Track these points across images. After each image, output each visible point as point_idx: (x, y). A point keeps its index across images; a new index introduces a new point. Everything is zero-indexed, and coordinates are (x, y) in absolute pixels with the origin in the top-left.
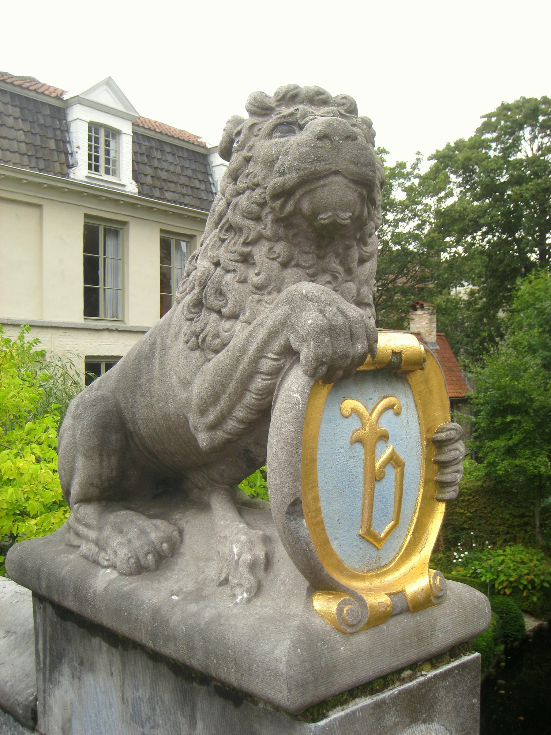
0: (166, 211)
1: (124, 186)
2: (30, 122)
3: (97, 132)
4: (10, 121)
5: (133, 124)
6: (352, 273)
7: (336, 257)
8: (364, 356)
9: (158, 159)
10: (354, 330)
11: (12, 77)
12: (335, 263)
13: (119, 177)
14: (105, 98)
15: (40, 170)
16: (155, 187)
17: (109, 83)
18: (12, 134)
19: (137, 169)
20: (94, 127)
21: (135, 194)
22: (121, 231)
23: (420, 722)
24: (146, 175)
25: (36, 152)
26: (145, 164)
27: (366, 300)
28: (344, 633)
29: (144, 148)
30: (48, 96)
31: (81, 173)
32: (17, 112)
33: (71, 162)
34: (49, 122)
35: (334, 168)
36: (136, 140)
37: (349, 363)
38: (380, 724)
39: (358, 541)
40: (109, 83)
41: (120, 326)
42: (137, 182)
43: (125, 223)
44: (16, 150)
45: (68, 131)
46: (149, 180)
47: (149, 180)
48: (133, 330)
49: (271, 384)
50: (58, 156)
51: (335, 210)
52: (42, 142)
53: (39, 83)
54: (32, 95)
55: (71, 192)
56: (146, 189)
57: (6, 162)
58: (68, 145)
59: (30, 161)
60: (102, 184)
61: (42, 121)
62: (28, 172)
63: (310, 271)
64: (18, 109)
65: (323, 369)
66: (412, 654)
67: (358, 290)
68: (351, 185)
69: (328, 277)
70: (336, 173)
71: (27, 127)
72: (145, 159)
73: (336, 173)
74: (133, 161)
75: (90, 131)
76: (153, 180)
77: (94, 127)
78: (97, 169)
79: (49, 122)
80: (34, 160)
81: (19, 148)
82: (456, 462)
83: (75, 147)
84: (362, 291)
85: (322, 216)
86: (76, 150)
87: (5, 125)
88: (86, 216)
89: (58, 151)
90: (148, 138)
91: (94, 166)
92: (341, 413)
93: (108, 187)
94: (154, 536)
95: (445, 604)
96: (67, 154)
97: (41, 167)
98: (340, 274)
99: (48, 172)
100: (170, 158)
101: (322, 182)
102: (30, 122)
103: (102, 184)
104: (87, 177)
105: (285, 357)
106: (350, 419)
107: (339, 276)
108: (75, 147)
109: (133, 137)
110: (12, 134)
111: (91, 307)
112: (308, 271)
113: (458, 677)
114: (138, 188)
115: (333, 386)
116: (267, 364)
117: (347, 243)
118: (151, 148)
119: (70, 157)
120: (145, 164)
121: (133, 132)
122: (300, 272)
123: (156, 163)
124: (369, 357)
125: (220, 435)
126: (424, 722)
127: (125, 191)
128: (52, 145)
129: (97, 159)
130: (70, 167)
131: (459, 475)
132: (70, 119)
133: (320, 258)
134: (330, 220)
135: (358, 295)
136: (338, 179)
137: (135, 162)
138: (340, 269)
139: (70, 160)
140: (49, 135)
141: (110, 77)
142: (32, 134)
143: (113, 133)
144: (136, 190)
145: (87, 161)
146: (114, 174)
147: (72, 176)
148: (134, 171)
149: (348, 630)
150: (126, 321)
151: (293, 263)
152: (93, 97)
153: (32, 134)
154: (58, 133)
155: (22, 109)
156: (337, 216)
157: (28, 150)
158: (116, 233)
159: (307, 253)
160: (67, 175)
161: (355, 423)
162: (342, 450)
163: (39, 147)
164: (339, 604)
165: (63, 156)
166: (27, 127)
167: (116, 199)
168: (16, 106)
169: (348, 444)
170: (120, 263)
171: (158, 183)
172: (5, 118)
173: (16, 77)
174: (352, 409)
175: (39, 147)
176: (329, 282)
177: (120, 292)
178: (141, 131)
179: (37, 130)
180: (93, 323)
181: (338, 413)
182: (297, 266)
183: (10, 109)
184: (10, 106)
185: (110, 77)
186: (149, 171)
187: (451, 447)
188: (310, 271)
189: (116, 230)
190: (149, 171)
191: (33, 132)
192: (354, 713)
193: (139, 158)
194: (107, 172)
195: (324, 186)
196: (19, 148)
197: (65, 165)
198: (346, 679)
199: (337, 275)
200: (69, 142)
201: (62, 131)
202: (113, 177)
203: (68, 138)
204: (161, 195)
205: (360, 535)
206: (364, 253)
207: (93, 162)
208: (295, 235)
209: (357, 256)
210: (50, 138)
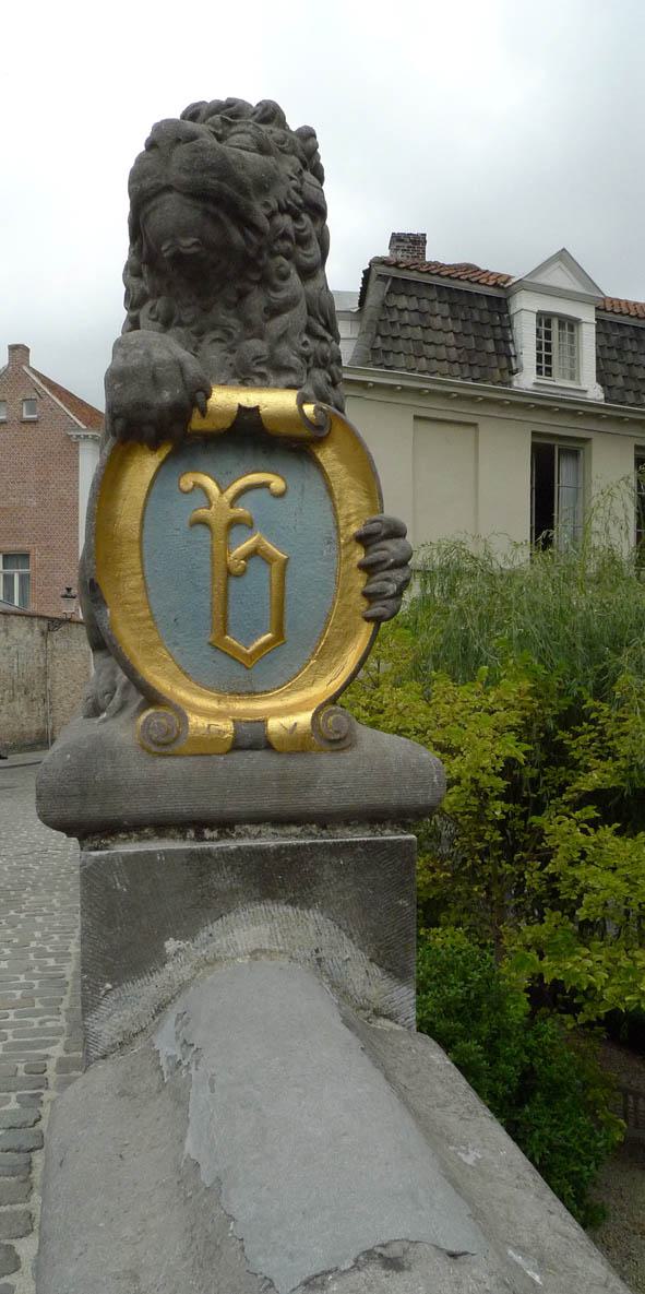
0: (599, 415)
1: (585, 391)
2: (462, 320)
3: (548, 324)
4: (437, 322)
5: (597, 309)
9: (633, 353)
10: (159, 375)
11: (443, 266)
13: (579, 380)
14: (559, 278)
15: (474, 380)
16: (628, 391)
17: (563, 256)
18: (439, 338)
19: (602, 367)
20: (544, 319)
23: (283, 902)
25: (470, 357)
26: (615, 360)
27: (285, 363)
28: (149, 751)
29: (613, 339)
30: (484, 284)
31: (526, 378)
32: (445, 310)
33: (514, 368)
34: (486, 317)
35: (164, 182)
36: (601, 330)
38: (201, 882)
39: (208, 651)
40: (563, 256)
42: (602, 386)
43: (586, 441)
44: (445, 357)
45: (510, 327)
46: (620, 381)
50: (498, 360)
51: (173, 236)
52: (477, 345)
53: (479, 270)
54: (464, 286)
55: (514, 405)
56: (616, 394)
57: (432, 373)
58: (511, 345)
59: (471, 371)
60: (572, 393)
61: (477, 318)
62: (458, 383)
63: (194, 328)
64: (447, 306)
66: (268, 803)
68: (189, 202)
69: (217, 334)
70: (168, 188)
71: (458, 327)
72: (615, 354)
73: (168, 188)
74: (598, 358)
75: (539, 322)
76: (625, 382)
77: (544, 319)
78: (549, 371)
79: (486, 317)
80: (466, 367)
81: (448, 355)
85: (163, 248)
87: (430, 327)
88: (534, 434)
89: (498, 353)
90: (620, 326)
91: (545, 365)
92: (180, 489)
95: (348, 755)
96: (509, 357)
97: (476, 376)
98: (233, 328)
99: (484, 382)
101: (153, 204)
102: (462, 320)
103: (554, 391)
104: (535, 384)
107: (234, 332)
109: (597, 326)
110: (439, 338)
113: (364, 858)
114: (604, 392)
118: (623, 338)
119: (513, 360)
120: (615, 360)
121: (596, 319)
123: (630, 358)
126: (292, 902)
128: (490, 346)
130: (512, 373)
131: (391, 585)
132: (513, 311)
133: (206, 310)
136: (172, 196)
137: (600, 359)
138: (233, 321)
139: (514, 365)
140: (487, 335)
141: (564, 250)
142: (465, 335)
143: (570, 324)
144: (602, 396)
145: (535, 363)
147: (515, 384)
148: (599, 371)
149: (154, 749)
151: (175, 321)
152: (542, 279)
153: (465, 335)
154: (498, 331)
155: (452, 305)
157: (460, 356)
158: (575, 454)
159: (188, 305)
160: (509, 383)
162: (178, 533)
163: (473, 352)
165: (504, 359)
166: (458, 327)
168: (445, 302)
169: (187, 525)
171: (632, 385)
172: (431, 318)
173: (448, 266)
175: (473, 352)
176: (220, 340)
178: (608, 317)
179: (471, 329)
182: (181, 324)
183: (437, 307)
184: (436, 303)
185: (564, 250)
187: (378, 546)
188: (194, 328)
189: (575, 449)
190: (619, 368)
191: (466, 332)
192: (151, 854)
193: (607, 354)
195: (155, 208)
196: (448, 355)
197: (507, 371)
198: (142, 807)
199: (231, 330)
200: (512, 341)
201: (503, 328)
203: (510, 337)
204: (637, 400)
206: (273, 301)
210: (487, 339)
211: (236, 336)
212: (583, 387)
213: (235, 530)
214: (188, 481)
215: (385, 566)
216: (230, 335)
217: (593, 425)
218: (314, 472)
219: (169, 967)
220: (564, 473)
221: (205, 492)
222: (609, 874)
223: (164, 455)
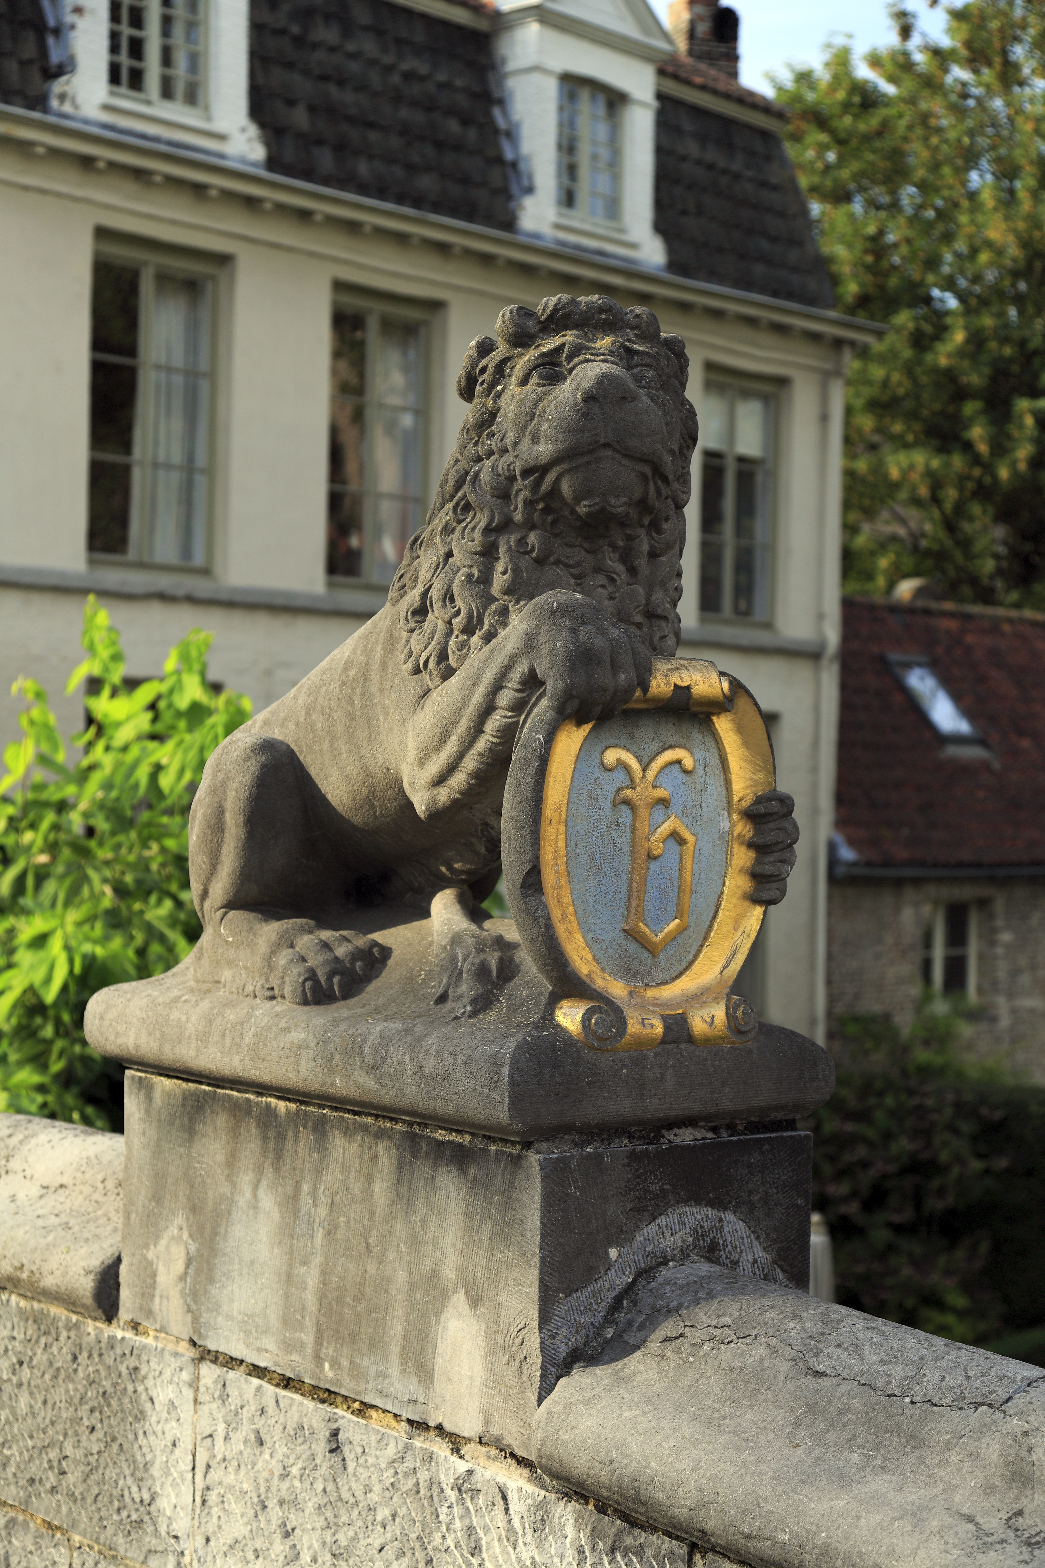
1: (221, 137)
6: (636, 574)
7: (614, 552)
8: (630, 691)
12: (611, 559)
13: (207, 108)
21: (255, 164)
22: (209, 286)
24: (291, 103)
27: (659, 611)
37: (608, 697)
41: (200, 586)
43: (224, 260)
46: (300, 118)
47: (300, 118)
48: (238, 598)
49: (512, 723)
65: (574, 705)
67: (648, 596)
78: (136, 80)
82: (780, 846)
83: (69, 9)
84: (653, 598)
86: (70, 18)
88: (102, 233)
91: (125, 75)
92: (602, 763)
93: (170, 143)
94: (341, 951)
100: (369, 46)
105: (531, 688)
106: (615, 773)
108: (69, 9)
111: (109, 526)
112: (572, 570)
114: (268, 144)
115: (593, 729)
116: (505, 698)
117: (628, 532)
119: (51, 41)
122: (561, 572)
124: (638, 693)
125: (444, 795)
127: (222, 156)
129: (137, 48)
134: (597, 507)
135: (647, 604)
137: (260, 58)
138: (620, 568)
144: (258, 153)
146: (192, 97)
150: (218, 569)
151: (552, 559)
156: (608, 502)
159: (570, 546)
161: (620, 777)
164: (587, 1010)
165: (30, 36)
167: (190, 176)
170: (204, 386)
174: (618, 760)
177: (199, 478)
180: (113, 577)
181: (596, 763)
182: (558, 562)
186: (301, 85)
189: (199, 278)
194: (167, 92)
202: (188, 110)
205: (624, 931)
207: (124, 59)
208: (554, 523)
209: (646, 547)
211: (619, 582)
212: (219, 125)
213: (660, 807)
214: (611, 756)
215: (780, 846)
216: (612, 580)
217: (237, 223)
218: (709, 739)
219: (612, 1274)
220: (162, 330)
221: (627, 768)
222: (80, 1358)
223: (587, 731)
